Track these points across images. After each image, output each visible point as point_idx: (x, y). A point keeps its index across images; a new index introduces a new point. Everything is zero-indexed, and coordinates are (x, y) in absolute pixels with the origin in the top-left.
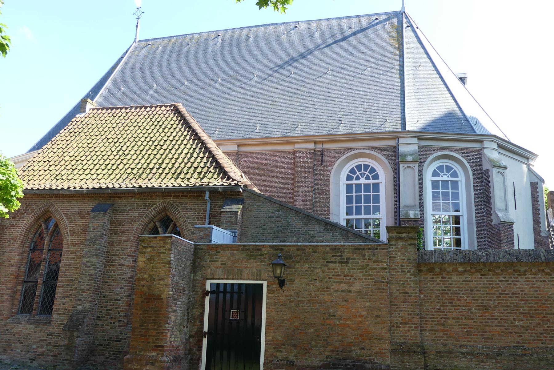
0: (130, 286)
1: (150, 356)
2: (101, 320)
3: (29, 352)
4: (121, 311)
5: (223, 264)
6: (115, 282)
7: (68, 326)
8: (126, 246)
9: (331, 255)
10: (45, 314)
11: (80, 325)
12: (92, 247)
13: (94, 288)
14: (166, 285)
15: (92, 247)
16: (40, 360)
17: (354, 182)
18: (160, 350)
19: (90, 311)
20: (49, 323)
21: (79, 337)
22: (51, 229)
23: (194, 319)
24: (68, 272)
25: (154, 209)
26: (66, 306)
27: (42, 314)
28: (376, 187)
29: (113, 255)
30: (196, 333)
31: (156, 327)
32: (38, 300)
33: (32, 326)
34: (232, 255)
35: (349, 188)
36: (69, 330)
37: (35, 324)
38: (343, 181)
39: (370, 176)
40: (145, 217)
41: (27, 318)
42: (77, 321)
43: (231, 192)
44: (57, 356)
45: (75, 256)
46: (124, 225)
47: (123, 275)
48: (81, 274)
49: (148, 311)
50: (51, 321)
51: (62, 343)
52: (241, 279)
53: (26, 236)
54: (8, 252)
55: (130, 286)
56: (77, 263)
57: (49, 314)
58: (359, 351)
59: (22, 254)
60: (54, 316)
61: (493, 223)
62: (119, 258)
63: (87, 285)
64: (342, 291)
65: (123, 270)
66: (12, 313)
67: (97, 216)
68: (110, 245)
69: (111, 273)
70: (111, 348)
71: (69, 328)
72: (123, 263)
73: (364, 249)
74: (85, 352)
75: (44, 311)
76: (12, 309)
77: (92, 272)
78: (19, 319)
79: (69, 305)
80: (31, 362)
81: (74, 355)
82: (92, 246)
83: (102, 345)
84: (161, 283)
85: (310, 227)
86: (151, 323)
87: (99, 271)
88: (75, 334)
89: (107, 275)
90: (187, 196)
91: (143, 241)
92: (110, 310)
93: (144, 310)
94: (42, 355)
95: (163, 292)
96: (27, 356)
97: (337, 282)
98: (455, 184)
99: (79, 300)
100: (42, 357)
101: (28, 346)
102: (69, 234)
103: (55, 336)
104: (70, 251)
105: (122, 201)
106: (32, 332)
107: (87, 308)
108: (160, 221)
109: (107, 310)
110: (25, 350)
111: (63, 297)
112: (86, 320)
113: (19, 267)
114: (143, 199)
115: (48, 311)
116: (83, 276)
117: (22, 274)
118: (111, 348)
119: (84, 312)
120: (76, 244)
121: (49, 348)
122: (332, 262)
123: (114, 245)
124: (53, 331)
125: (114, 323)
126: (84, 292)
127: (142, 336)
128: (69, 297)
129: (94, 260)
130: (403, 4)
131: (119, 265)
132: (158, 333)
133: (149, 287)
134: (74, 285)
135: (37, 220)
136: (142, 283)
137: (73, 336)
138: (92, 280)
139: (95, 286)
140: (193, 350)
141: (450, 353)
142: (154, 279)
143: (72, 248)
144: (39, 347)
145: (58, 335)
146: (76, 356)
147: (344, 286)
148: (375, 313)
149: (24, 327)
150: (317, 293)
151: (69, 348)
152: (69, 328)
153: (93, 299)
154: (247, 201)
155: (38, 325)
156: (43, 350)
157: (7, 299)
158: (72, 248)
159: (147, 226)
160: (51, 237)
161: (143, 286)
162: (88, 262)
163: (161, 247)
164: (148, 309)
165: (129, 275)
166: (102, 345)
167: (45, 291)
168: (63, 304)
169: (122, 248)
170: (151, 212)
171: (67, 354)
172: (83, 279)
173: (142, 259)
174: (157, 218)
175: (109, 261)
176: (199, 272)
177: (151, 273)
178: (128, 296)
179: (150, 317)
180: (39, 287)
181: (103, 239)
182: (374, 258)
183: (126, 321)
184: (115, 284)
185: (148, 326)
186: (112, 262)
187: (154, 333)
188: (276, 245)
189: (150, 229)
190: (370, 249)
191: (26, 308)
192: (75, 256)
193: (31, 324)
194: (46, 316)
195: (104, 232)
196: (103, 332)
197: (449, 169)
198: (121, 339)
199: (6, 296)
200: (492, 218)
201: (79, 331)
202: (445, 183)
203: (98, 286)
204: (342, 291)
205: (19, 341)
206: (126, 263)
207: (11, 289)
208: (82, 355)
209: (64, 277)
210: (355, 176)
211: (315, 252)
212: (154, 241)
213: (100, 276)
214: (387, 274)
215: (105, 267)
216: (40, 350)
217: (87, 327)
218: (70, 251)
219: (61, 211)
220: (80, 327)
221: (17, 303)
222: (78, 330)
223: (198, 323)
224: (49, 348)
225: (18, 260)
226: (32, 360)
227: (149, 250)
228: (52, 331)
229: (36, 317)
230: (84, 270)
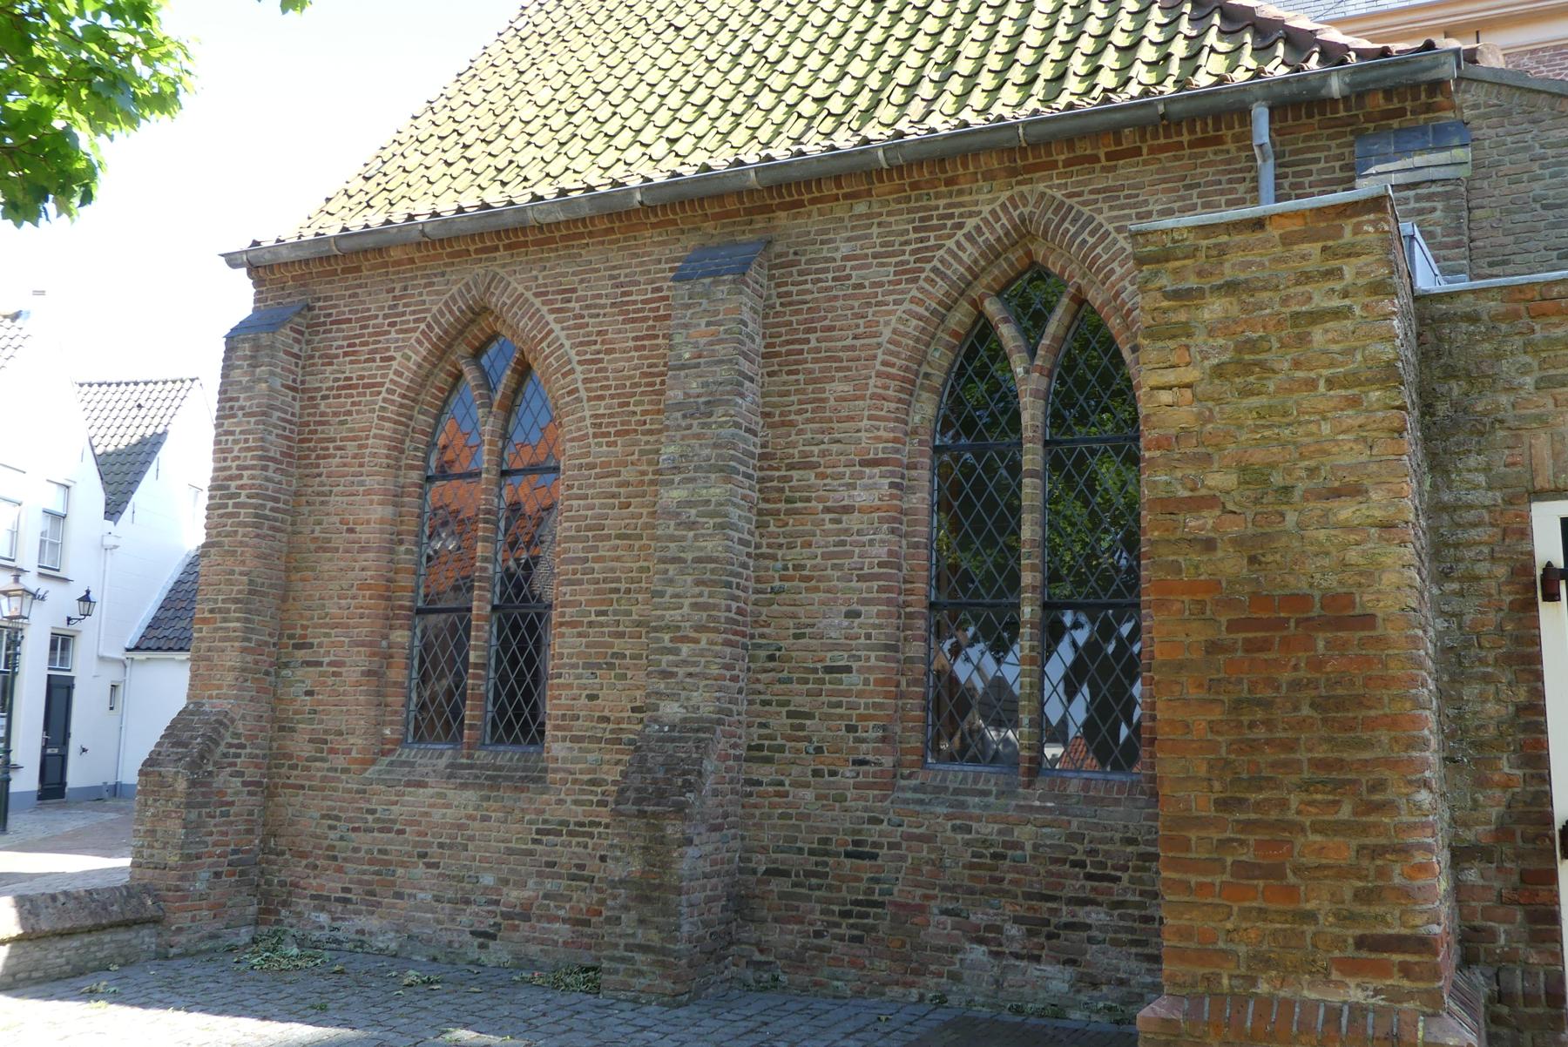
0: (889, 602)
1: (1333, 1014)
2: (768, 760)
3: (467, 902)
4: (862, 718)
6: (816, 589)
7: (631, 795)
8: (850, 419)
10: (516, 742)
11: (688, 786)
12: (697, 436)
13: (729, 621)
14: (1386, 526)
15: (697, 436)
16: (516, 936)
18: (1406, 970)
19: (720, 722)
20: (535, 778)
21: (689, 842)
22: (501, 388)
23: (1479, 745)
24: (595, 560)
25: (969, 237)
26: (605, 705)
27: (500, 741)
29: (791, 467)
30: (1503, 832)
31: (1345, 812)
32: (480, 684)
33: (471, 795)
36: (642, 814)
37: (481, 787)
40: (929, 280)
41: (443, 762)
42: (669, 767)
43: (1388, 93)
44: (587, 923)
45: (620, 485)
46: (831, 329)
47: (850, 555)
48: (663, 561)
49: (1267, 704)
50: (545, 770)
51: (617, 871)
53: (404, 420)
54: (342, 494)
55: (889, 602)
56: (633, 516)
57: (533, 742)
59: (395, 498)
60: (556, 748)
62: (823, 476)
63: (695, 606)
65: (846, 531)
66: (384, 741)
67: (707, 295)
68: (772, 426)
69: (791, 546)
70: (830, 887)
71: (637, 802)
72: (844, 497)
74: (717, 907)
75: (509, 727)
76: (380, 724)
77: (713, 546)
78: (412, 765)
79: (616, 699)
80: (482, 946)
81: (678, 927)
82: (696, 429)
83: (786, 874)
84: (1346, 511)
86: (1305, 786)
87: (742, 542)
88: (673, 830)
89: (774, 558)
90: (1137, 152)
91: (1164, 257)
92: (810, 716)
93: (1237, 706)
94: (525, 913)
95: (1369, 573)
96: (464, 919)
99: (666, 675)
100: (524, 926)
101: (461, 880)
102: (583, 394)
103: (571, 834)
104: (593, 466)
105: (811, 222)
106: (470, 817)
107: (707, 710)
108: (999, 294)
109: (790, 715)
110: (450, 894)
111: (587, 666)
112: (708, 766)
113: (392, 551)
114: (908, 199)
115: (525, 729)
116: (672, 568)
118: (830, 887)
119: (696, 730)
120: (617, 434)
121: (549, 885)
123: (792, 424)
124: (560, 813)
125: (833, 773)
126: (685, 639)
127: (1242, 869)
128: (611, 666)
129: (716, 491)
131: (827, 510)
132: (1377, 852)
133: (1254, 550)
134: (628, 613)
135: (441, 352)
136: (1201, 523)
137: (662, 841)
138: (714, 583)
139: (729, 609)
140: (1492, 936)
142: (1287, 490)
143: (600, 451)
144: (506, 882)
145: (580, 830)
146: (686, 928)
149: (436, 799)
151: (651, 893)
152: (637, 802)
153: (727, 667)
154: (1485, 132)
155: (491, 788)
156: (527, 894)
157: (358, 684)
158: (600, 451)
159: (943, 319)
160: (507, 421)
161: (1209, 545)
162: (690, 504)
163: (1305, 277)
164: (1269, 693)
165: (881, 552)
166: (786, 874)
167: (505, 645)
168: (592, 697)
169: (830, 431)
170: (958, 251)
171: (642, 922)
172: (671, 582)
173: (1171, 377)
174: (986, 280)
175: (775, 490)
176: (1472, 461)
177: (1258, 457)
178: (887, 647)
179: (1290, 746)
180: (479, 628)
181: (742, 396)
183: (888, 761)
184: (816, 596)
185: (1283, 804)
186: (788, 501)
187: (1343, 850)
189: (955, 334)
191: (437, 719)
192: (620, 485)
193: (464, 786)
194: (518, 749)
195: (745, 366)
196: (781, 816)
198: (875, 845)
199: (352, 673)
201: (686, 818)
203: (740, 612)
205: (424, 855)
206: (861, 497)
207: (371, 644)
208: (706, 924)
209: (580, 582)
212: (1245, 248)
213: (745, 566)
215: (761, 525)
216: (514, 895)
217: (715, 793)
218: (592, 466)
219: (537, 302)
220: (690, 796)
221: (396, 701)
222: (680, 810)
223: (1506, 766)
224: (549, 885)
225: (382, 521)
226: (486, 936)
227: (1215, 309)
228: (555, 813)
229: (481, 756)
230: (672, 538)
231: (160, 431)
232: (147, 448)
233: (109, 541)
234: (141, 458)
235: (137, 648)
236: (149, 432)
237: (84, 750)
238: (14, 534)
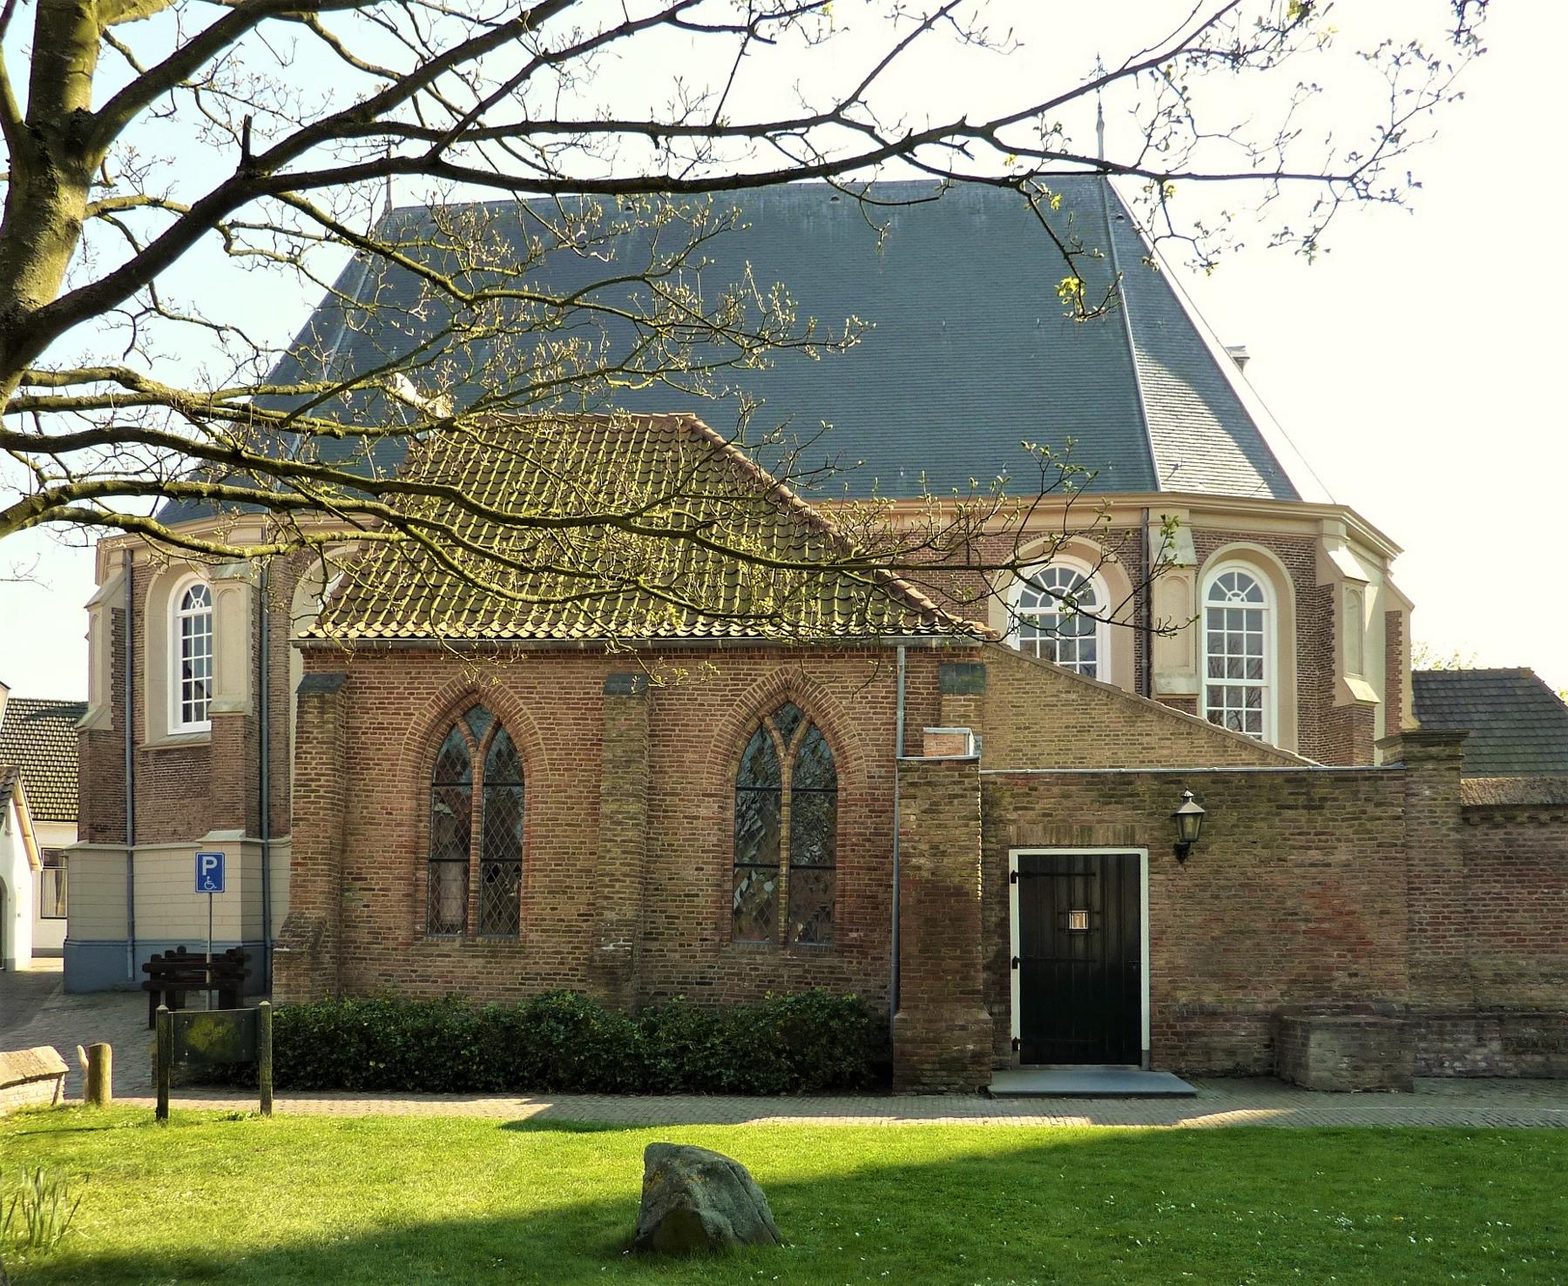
5: (1045, 815)
9: (1286, 792)
26: (561, 913)
34: (1066, 796)
52: (1089, 846)
58: (1347, 980)
61: (1336, 704)
64: (1312, 865)
66: (416, 932)
72: (694, 811)
73: (1355, 780)
85: (1141, 726)
97: (1302, 847)
98: (1255, 618)
117: (425, 843)
122: (1289, 807)
124: (536, 969)
141: (1521, 975)
143: (554, 778)
147: (1315, 855)
148: (1378, 907)
150: (1257, 870)
158: (554, 778)
165: (715, 840)
170: (754, 694)
177: (936, 839)
182: (1377, 798)
188: (1165, 773)
190: (1367, 779)
197: (1244, 581)
200: (1334, 692)
202: (1235, 614)
204: (1312, 865)
206: (703, 812)
211: (1252, 787)
214: (1400, 829)
219: (512, 692)
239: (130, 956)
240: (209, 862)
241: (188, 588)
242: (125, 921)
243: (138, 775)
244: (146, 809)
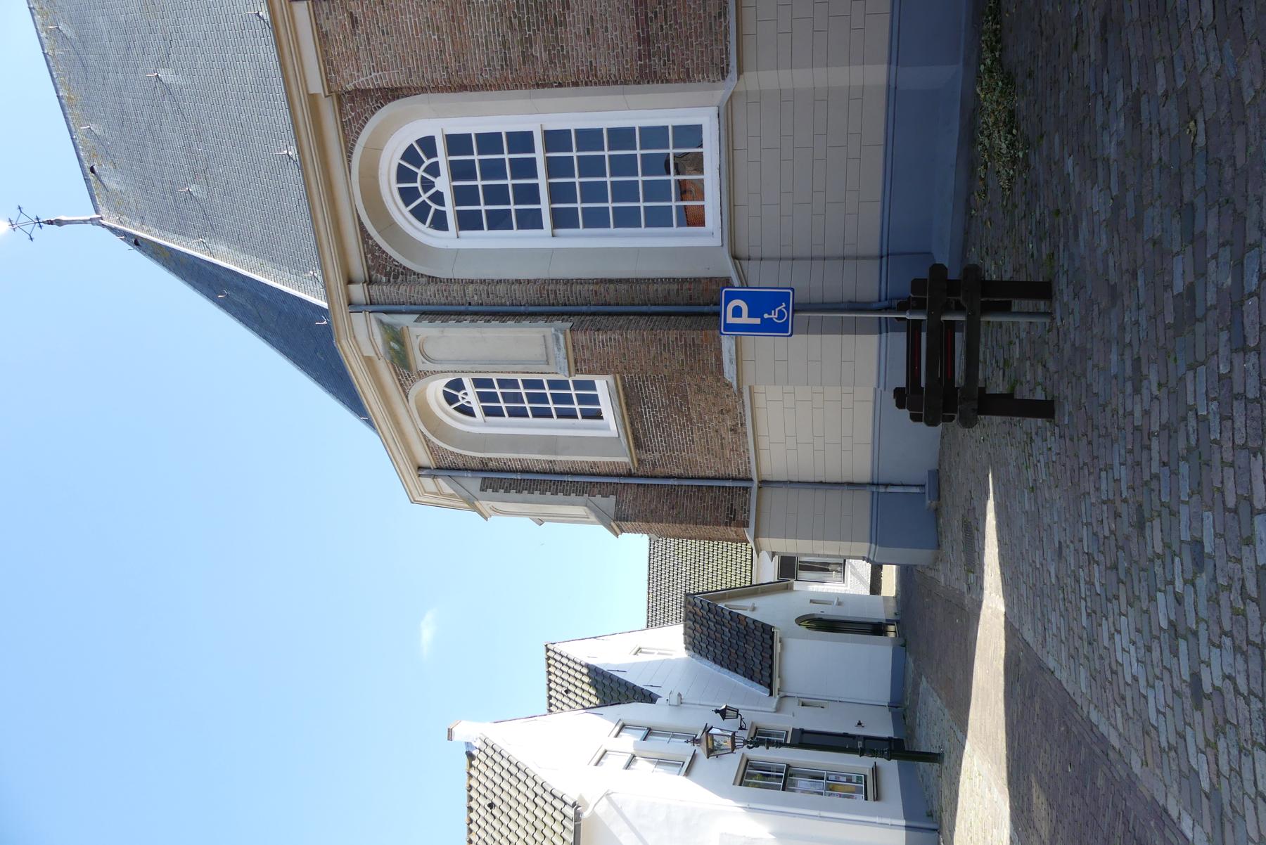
17: (450, 208)
28: (457, 143)
35: (468, 222)
38: (451, 239)
39: (427, 162)
130: (85, 222)
210: (434, 207)
231: (585, 671)
232: (599, 679)
233: (674, 700)
234: (607, 683)
235: (770, 686)
236: (586, 679)
237: (860, 724)
238: (660, 762)
239: (890, 489)
240: (737, 312)
241: (450, 409)
242: (847, 494)
243: (667, 471)
244: (707, 464)
